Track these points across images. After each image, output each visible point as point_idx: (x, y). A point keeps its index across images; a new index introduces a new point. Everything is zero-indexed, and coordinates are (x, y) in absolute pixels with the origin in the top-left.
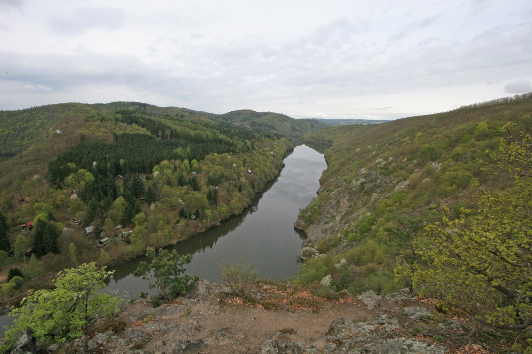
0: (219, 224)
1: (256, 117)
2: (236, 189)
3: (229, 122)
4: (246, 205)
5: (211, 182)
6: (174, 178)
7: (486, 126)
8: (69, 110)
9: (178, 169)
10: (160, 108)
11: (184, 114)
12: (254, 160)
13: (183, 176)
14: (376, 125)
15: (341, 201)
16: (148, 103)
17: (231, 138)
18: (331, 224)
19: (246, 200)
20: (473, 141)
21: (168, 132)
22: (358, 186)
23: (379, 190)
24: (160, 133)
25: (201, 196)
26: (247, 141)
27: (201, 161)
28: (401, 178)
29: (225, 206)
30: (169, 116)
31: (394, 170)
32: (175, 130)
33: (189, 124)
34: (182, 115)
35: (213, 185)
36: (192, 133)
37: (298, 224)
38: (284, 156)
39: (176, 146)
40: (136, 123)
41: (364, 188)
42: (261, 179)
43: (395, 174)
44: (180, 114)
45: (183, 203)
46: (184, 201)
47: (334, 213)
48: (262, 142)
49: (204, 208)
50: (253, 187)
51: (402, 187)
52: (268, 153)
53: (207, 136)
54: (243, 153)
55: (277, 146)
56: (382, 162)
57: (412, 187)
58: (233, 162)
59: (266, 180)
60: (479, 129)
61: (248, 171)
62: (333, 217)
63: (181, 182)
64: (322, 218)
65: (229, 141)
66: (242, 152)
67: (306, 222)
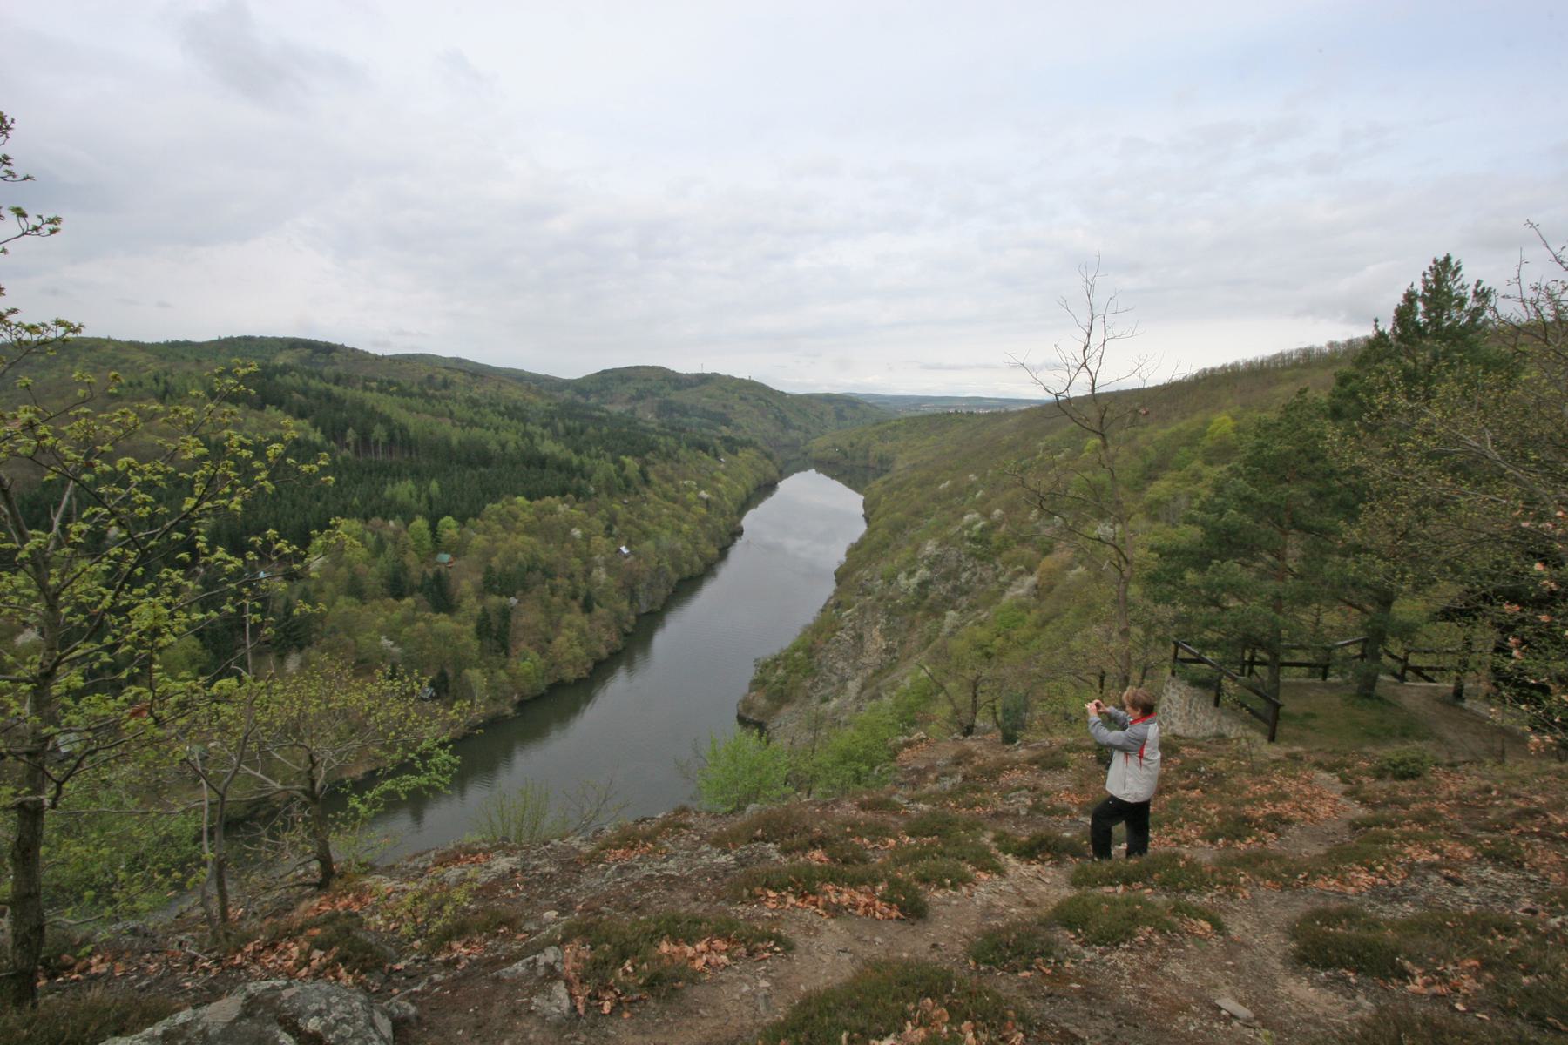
0: (510, 711)
1: (677, 389)
2: (575, 605)
3: (593, 400)
4: (604, 652)
5: (493, 583)
6: (373, 575)
7: (1231, 423)
8: (73, 361)
9: (390, 545)
10: (376, 357)
11: (450, 376)
12: (642, 515)
13: (405, 568)
14: (1007, 414)
15: (866, 635)
16: (339, 343)
17: (578, 452)
18: (835, 702)
19: (606, 637)
20: (1197, 464)
21: (379, 432)
22: (911, 591)
23: (964, 601)
24: (351, 435)
25: (457, 628)
26: (627, 460)
27: (471, 520)
28: (1021, 567)
29: (534, 655)
30: (398, 384)
31: (1005, 545)
32: (403, 429)
33: (456, 408)
34: (445, 381)
35: (500, 595)
36: (456, 435)
37: (747, 705)
38: (747, 504)
39: (398, 475)
40: (279, 404)
41: (926, 597)
42: (658, 572)
43: (1005, 555)
44: (440, 378)
45: (396, 650)
46: (398, 643)
47: (848, 670)
48: (678, 461)
49: (461, 663)
50: (633, 597)
51: (1021, 591)
52: (691, 496)
53: (503, 446)
54: (610, 495)
55: (725, 474)
56: (975, 522)
57: (1040, 592)
58: (573, 525)
59: (675, 577)
60: (1212, 432)
61: (619, 551)
62: (844, 680)
63: (397, 587)
64: (814, 685)
65: (569, 461)
66: (604, 495)
67: (769, 698)
